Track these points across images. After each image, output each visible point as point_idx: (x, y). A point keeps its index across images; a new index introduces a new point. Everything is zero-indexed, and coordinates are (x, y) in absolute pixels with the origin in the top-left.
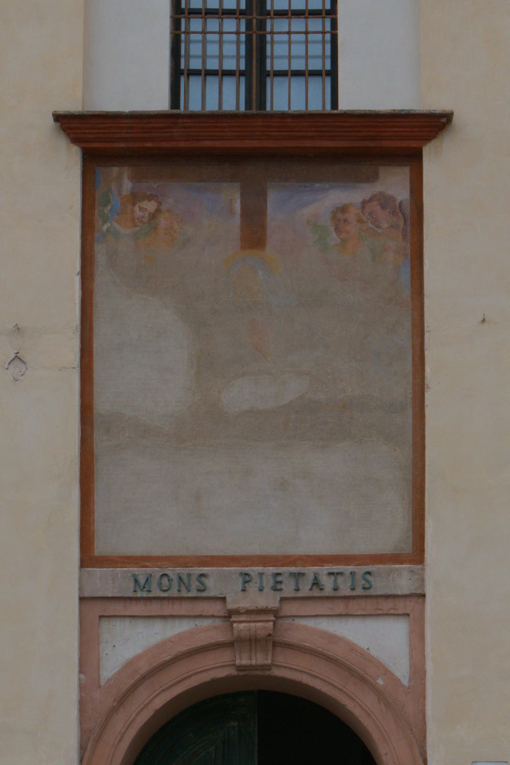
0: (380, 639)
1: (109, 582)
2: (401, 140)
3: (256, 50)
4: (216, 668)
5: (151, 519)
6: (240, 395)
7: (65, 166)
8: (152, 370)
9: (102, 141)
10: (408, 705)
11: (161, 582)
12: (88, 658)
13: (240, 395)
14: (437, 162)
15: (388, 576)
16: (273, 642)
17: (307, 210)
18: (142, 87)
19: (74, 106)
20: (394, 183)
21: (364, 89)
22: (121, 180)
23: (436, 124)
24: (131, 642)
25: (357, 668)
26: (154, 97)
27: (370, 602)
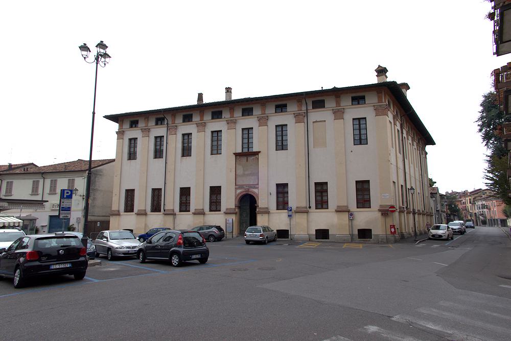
0: (256, 191)
1: (237, 187)
2: (257, 153)
3: (355, 93)
4: (244, 193)
5: (240, 183)
6: (246, 173)
7: (234, 156)
8: (240, 172)
9: (236, 155)
10: (258, 195)
11: (241, 187)
12: (236, 191)
13: (246, 173)
14: (375, 115)
15: (256, 186)
16: (248, 191)
17: (251, 158)
18: (239, 150)
19: (234, 152)
20: (257, 156)
21: (255, 150)
22: (238, 157)
23: (260, 152)
24: (239, 191)
25: (254, 193)
26: (240, 151)
27: (255, 188)
